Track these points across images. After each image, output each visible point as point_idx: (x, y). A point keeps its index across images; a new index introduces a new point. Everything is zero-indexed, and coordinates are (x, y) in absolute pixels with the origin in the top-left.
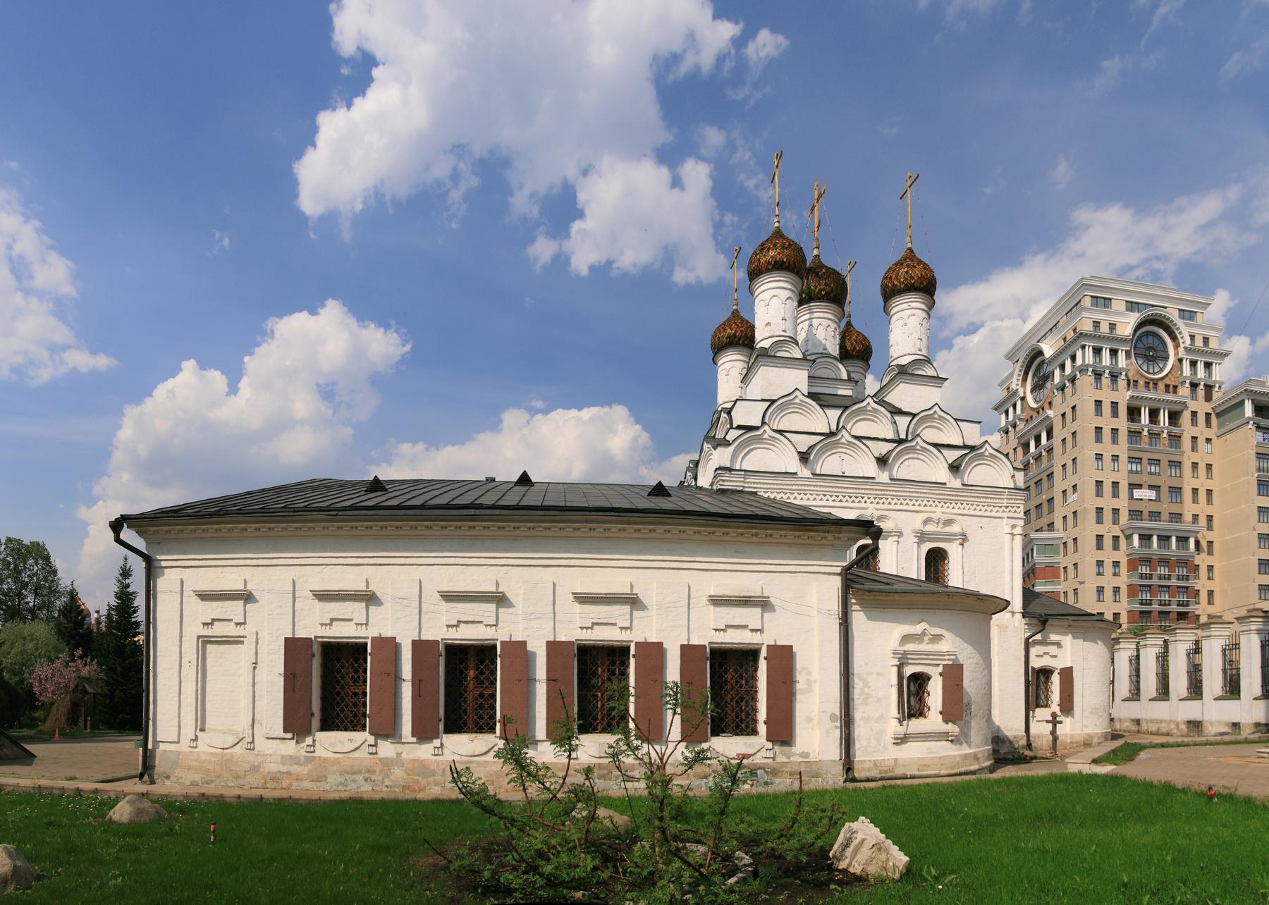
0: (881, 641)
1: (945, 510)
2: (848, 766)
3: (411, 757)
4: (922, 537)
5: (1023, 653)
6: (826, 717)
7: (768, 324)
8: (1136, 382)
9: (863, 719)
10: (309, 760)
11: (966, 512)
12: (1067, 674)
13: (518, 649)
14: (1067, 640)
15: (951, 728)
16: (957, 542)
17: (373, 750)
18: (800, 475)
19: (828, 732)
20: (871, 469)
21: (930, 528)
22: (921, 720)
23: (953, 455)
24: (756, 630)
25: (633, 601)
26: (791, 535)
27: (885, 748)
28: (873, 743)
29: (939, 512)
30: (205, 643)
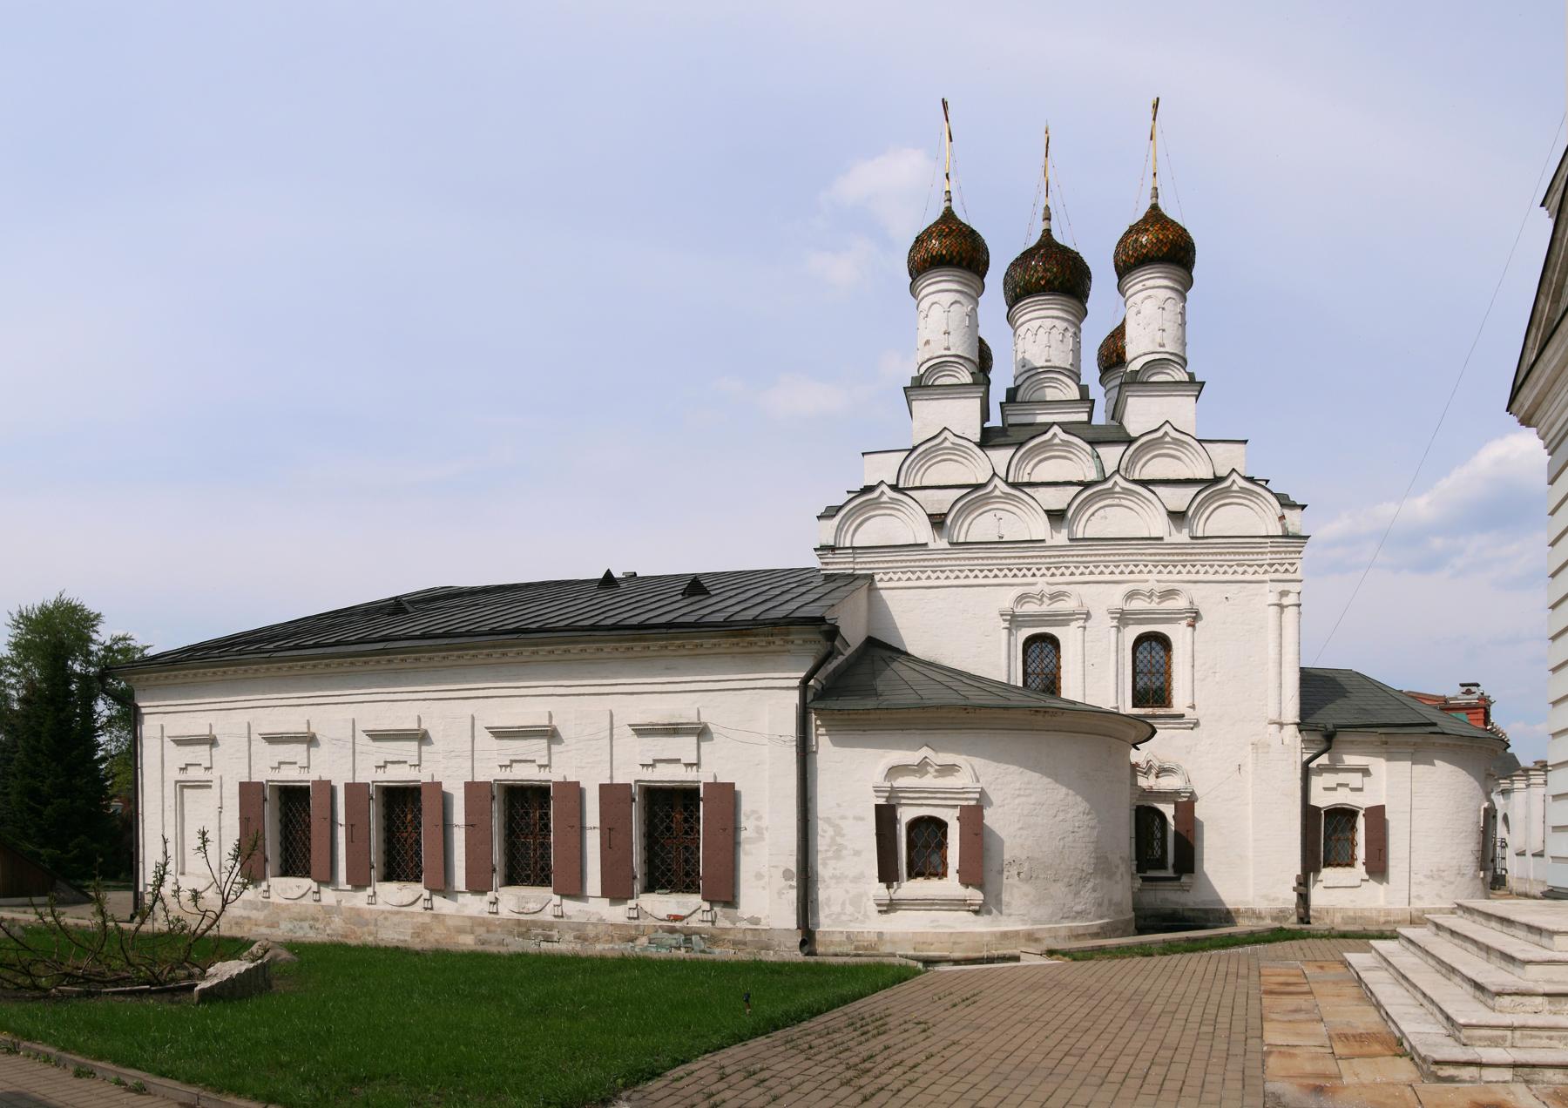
0: (856, 775)
1: (1160, 577)
2: (808, 938)
3: (349, 905)
4: (1123, 618)
5: (1298, 784)
6: (779, 873)
7: (927, 342)
9: (833, 877)
10: (265, 905)
11: (1201, 577)
12: (1377, 816)
13: (574, 792)
14: (1378, 765)
15: (975, 895)
16: (1184, 623)
17: (317, 897)
18: (931, 546)
19: (780, 893)
20: (1039, 527)
21: (1030, 608)
22: (934, 882)
23: (1179, 498)
24: (691, 765)
25: (551, 735)
26: (726, 643)
27: (866, 916)
28: (849, 909)
29: (1153, 580)
30: (183, 787)
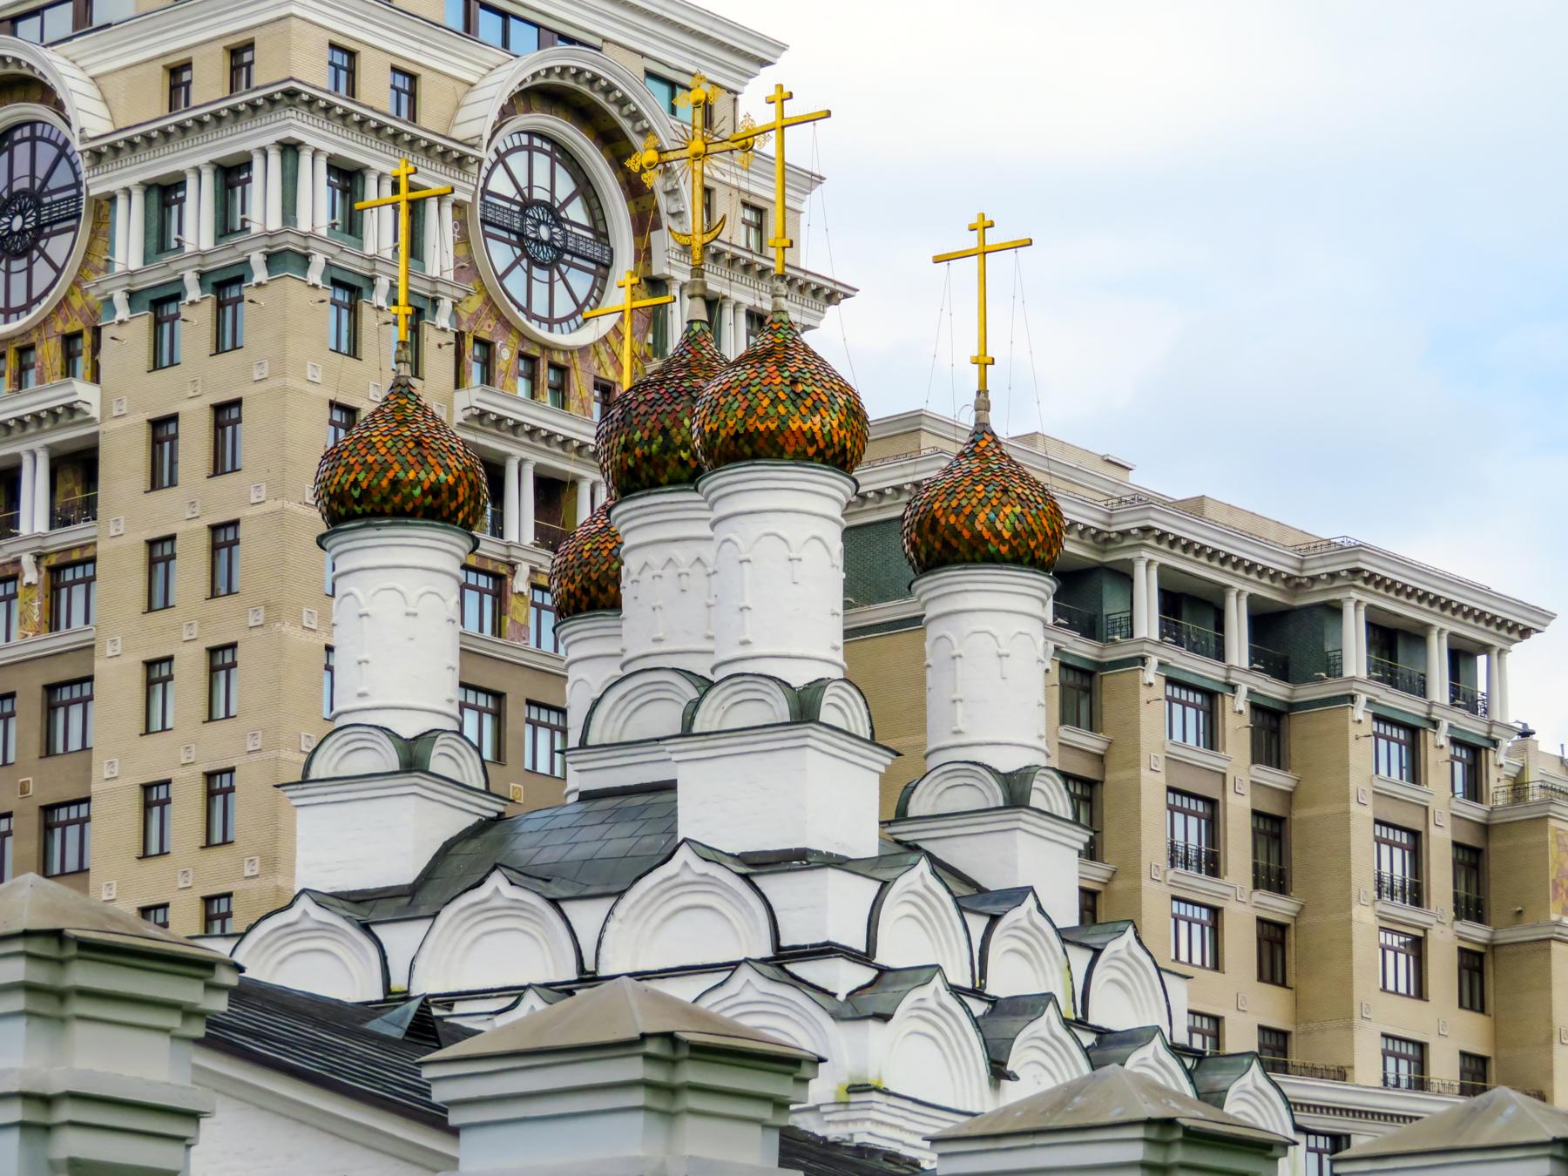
8: (486, 345)
